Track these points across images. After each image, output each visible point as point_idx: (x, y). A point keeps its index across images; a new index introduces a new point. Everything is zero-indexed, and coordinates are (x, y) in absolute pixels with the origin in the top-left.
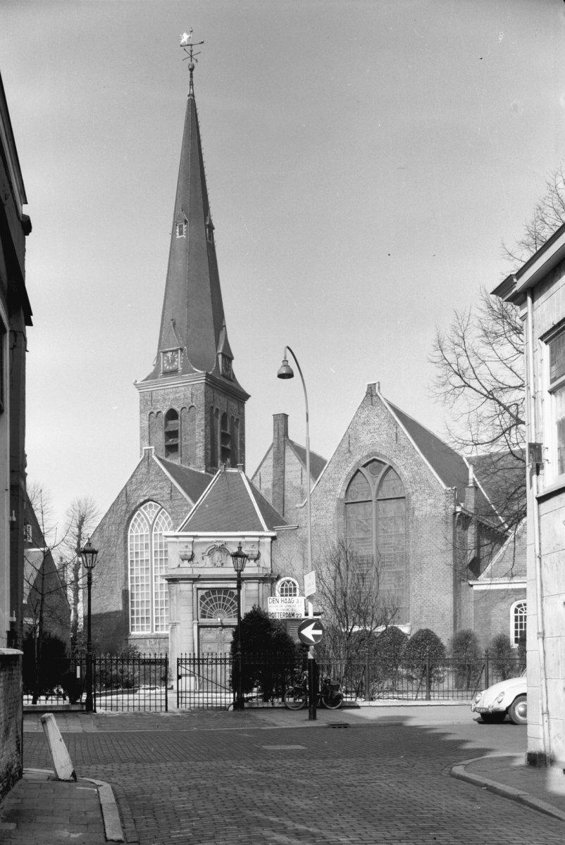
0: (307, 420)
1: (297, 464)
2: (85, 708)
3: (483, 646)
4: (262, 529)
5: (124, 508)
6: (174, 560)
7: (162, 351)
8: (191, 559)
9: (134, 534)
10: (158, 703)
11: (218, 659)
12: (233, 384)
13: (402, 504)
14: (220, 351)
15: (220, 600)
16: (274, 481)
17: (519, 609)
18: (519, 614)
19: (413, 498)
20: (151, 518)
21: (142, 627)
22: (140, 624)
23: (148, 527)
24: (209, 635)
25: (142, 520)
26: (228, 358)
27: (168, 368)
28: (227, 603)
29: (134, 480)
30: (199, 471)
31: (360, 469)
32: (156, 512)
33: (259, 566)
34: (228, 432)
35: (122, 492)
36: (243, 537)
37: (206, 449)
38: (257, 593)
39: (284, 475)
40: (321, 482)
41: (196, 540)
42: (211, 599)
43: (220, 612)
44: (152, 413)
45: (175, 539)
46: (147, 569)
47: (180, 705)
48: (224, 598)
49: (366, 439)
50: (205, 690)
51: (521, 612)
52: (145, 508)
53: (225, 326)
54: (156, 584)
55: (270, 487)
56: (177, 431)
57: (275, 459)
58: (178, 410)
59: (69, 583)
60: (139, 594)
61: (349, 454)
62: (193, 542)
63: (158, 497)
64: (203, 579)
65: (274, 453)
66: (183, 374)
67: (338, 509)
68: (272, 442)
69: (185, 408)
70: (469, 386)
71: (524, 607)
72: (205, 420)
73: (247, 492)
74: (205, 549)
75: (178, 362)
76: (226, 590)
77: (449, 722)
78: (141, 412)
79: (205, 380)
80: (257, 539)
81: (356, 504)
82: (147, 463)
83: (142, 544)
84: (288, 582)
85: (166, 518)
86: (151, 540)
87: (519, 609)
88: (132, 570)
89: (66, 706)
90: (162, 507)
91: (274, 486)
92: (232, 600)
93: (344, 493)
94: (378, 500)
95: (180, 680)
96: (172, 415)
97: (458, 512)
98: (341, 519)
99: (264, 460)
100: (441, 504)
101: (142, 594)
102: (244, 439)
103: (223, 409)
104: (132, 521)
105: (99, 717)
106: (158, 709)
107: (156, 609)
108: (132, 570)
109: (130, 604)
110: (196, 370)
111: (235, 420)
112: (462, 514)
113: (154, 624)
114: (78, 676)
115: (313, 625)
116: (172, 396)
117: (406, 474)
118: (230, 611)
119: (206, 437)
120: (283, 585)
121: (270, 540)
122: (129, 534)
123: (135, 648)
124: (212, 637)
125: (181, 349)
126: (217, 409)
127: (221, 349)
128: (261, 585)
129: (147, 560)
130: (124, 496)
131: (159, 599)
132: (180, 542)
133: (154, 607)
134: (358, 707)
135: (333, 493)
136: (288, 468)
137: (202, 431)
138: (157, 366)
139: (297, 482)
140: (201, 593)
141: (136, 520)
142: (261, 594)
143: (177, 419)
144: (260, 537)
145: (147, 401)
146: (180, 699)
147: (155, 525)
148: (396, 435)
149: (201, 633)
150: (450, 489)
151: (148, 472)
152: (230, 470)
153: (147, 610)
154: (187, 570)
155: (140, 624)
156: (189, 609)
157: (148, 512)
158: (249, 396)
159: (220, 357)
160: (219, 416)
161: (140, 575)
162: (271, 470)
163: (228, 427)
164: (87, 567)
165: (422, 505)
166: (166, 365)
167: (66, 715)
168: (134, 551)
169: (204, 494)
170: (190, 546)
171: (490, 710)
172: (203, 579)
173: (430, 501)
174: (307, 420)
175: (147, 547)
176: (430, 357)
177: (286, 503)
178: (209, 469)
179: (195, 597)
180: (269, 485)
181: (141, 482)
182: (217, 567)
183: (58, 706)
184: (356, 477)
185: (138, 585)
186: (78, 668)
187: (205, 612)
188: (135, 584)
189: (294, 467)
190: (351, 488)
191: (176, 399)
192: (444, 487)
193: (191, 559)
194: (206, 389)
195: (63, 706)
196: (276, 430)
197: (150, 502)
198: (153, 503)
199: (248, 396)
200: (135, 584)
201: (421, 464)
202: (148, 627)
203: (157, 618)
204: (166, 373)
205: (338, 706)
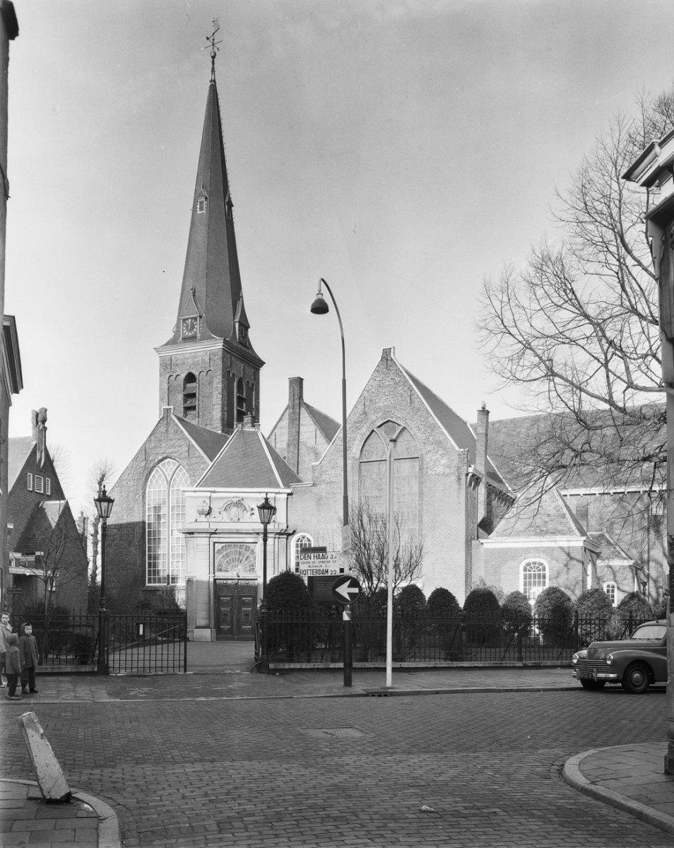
5: (143, 464)
41: (213, 495)
52: (163, 465)
82: (165, 422)
120: (298, 541)
122: (147, 490)
147: (172, 482)
151: (167, 431)
166: (185, 331)
204: (186, 339)
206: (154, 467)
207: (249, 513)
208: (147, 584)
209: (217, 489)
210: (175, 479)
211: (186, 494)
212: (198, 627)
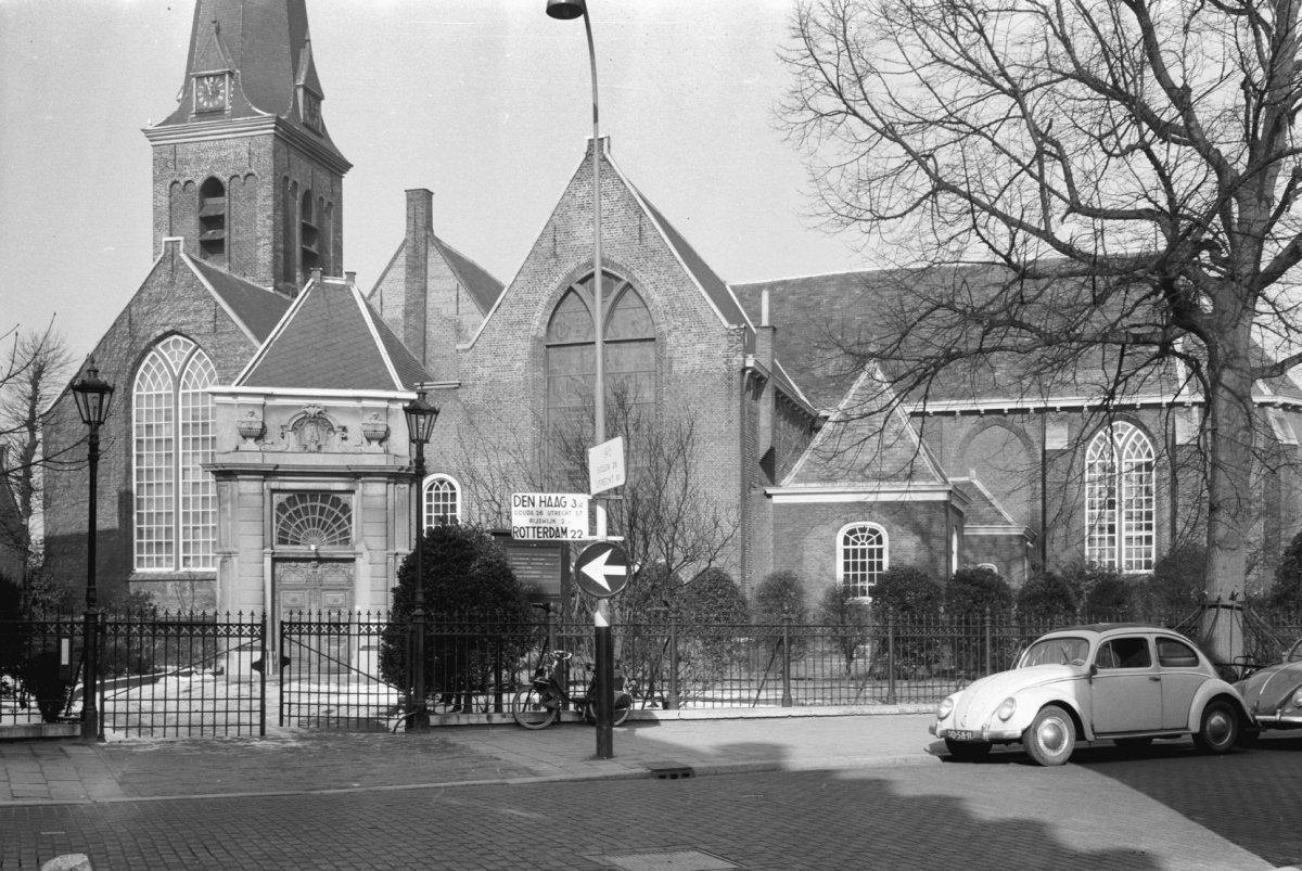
0: (596, 120)
2: (78, 732)
3: (815, 600)
4: (392, 387)
5: (126, 344)
6: (227, 438)
7: (194, 74)
8: (260, 436)
10: (245, 718)
11: (324, 624)
12: (323, 142)
13: (649, 349)
14: (301, 83)
15: (314, 512)
16: (406, 306)
17: (851, 538)
18: (851, 547)
19: (671, 340)
20: (176, 365)
22: (154, 555)
23: (170, 380)
24: (293, 576)
25: (160, 368)
26: (314, 95)
28: (327, 517)
29: (145, 295)
30: (263, 288)
31: (575, 287)
32: (187, 353)
33: (387, 452)
34: (313, 223)
35: (124, 312)
36: (359, 399)
37: (275, 250)
38: (382, 500)
39: (425, 296)
40: (502, 307)
41: (270, 402)
42: (306, 507)
43: (316, 534)
44: (175, 182)
45: (229, 399)
46: (169, 456)
47: (286, 719)
48: (322, 509)
49: (584, 233)
50: (296, 676)
51: (854, 543)
53: (309, 41)
54: (184, 483)
55: (400, 316)
56: (222, 216)
57: (408, 266)
58: (225, 179)
60: (151, 504)
61: (553, 260)
62: (264, 405)
63: (191, 327)
66: (232, 117)
67: (533, 354)
68: (403, 237)
70: (855, 114)
71: (859, 534)
72: (275, 199)
73: (363, 321)
75: (224, 95)
76: (326, 494)
77: (889, 759)
78: (155, 181)
79: (275, 129)
80: (384, 404)
81: (566, 349)
82: (169, 266)
83: (159, 412)
84: (442, 482)
85: (206, 365)
86: (177, 404)
87: (851, 538)
88: (139, 457)
89: (37, 727)
90: (199, 346)
91: (407, 314)
92: (291, 511)
93: (544, 328)
94: (606, 342)
95: (286, 668)
96: (213, 187)
97: (748, 368)
98: (539, 375)
99: (388, 269)
100: (720, 353)
102: (341, 238)
103: (304, 185)
104: (141, 370)
105: (118, 753)
106: (245, 730)
107: (184, 528)
108: (139, 457)
109: (135, 517)
110: (257, 110)
111: (325, 205)
112: (754, 372)
114: (65, 661)
115: (606, 555)
116: (213, 156)
117: (657, 299)
118: (333, 531)
119: (275, 228)
122: (135, 392)
123: (147, 597)
125: (231, 74)
126: (295, 183)
127: (303, 78)
128: (391, 485)
129: (169, 441)
131: (191, 510)
132: (239, 405)
133: (181, 525)
134: (656, 722)
135: (525, 327)
137: (268, 217)
138: (185, 102)
139: (449, 310)
140: (278, 498)
141: (147, 368)
142: (390, 503)
144: (390, 400)
145: (166, 162)
146: (286, 706)
147: (183, 379)
148: (640, 229)
149: (277, 571)
150: (736, 327)
151: (172, 283)
152: (329, 281)
153: (167, 529)
154: (252, 455)
155: (154, 555)
156: (256, 528)
157: (172, 354)
158: (351, 166)
159: (300, 92)
160: (298, 194)
161: (154, 467)
162: (402, 287)
163: (314, 214)
164: (88, 422)
165: (686, 353)
166: (201, 100)
167: (38, 748)
168: (145, 423)
169: (282, 321)
170: (259, 413)
171: (986, 735)
173: (701, 347)
174: (596, 120)
175: (168, 418)
176: (784, 53)
177: (429, 346)
178: (280, 285)
179: (267, 507)
180: (399, 314)
181: (158, 301)
182: (310, 452)
183: (16, 727)
184: (566, 300)
185: (150, 485)
186: (65, 643)
187: (286, 534)
189: (443, 287)
190: (556, 320)
191: (222, 161)
192: (726, 324)
193: (260, 436)
194: (275, 145)
195: (27, 728)
196: (411, 218)
197: (176, 337)
198: (180, 338)
199: (348, 166)
200: (145, 482)
201: (685, 281)
202: (169, 559)
204: (202, 114)
205: (622, 720)
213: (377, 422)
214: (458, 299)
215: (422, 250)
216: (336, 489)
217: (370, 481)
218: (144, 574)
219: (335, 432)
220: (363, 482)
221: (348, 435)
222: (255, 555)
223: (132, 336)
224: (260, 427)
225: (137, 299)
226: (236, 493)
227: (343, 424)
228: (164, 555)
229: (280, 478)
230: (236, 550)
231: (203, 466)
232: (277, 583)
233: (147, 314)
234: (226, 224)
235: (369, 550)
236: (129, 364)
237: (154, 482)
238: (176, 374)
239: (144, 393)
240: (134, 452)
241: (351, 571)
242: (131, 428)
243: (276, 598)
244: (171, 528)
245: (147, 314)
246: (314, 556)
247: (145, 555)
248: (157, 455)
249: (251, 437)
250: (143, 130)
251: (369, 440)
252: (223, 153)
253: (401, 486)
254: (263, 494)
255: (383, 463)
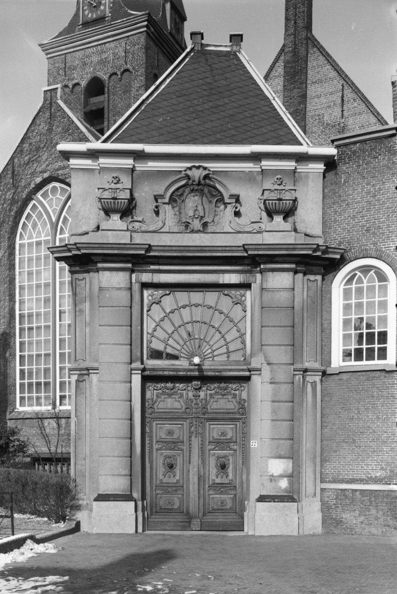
1: (332, 79)
5: (9, 195)
8: (127, 210)
9: (26, 241)
21: (38, 398)
22: (35, 395)
25: (40, 216)
27: (90, 16)
29: (26, 145)
41: (141, 167)
52: (45, 195)
57: (286, 73)
58: (105, 77)
59: (53, 411)
62: (133, 170)
64: (158, 260)
65: (286, 63)
68: (282, 42)
69: (115, 74)
74: (163, 189)
79: (147, 26)
82: (48, 114)
96: (96, 87)
101: (38, 342)
107: (61, 369)
110: (132, 12)
113: (58, 394)
116: (95, 59)
120: (350, 281)
121: (320, 167)
122: (18, 242)
123: (13, 433)
124: (177, 405)
128: (300, 275)
130: (10, 176)
136: (312, 91)
141: (29, 217)
143: (103, 93)
147: (60, 224)
149: (148, 395)
151: (50, 130)
155: (35, 395)
166: (86, 12)
170: (126, 182)
172: (158, 260)
181: (38, 149)
182: (193, 231)
185: (30, 329)
188: (26, 326)
198: (57, 185)
203: (62, 384)
204: (86, 24)
206: (29, 199)
207: (230, 210)
208: (21, 409)
209: (150, 148)
210: (65, 219)
211: (73, 162)
212: (101, 498)
213: (281, 187)
214: (343, 100)
215: (302, 51)
216: (226, 282)
217: (273, 270)
218: (25, 413)
219: (226, 204)
220: (261, 272)
221: (242, 210)
222: (121, 371)
223: (15, 186)
224: (128, 196)
225: (19, 151)
226: (96, 289)
227: (234, 191)
228: (43, 394)
229: (152, 267)
230: (95, 365)
231: (53, 250)
232: (148, 411)
233: (28, 163)
234: (106, 116)
235: (269, 364)
236: (13, 213)
237: (34, 325)
238: (54, 219)
239: (26, 241)
240: (17, 298)
241: (244, 395)
242: (14, 275)
243: (147, 429)
244: (49, 369)
245: (28, 163)
246: (196, 373)
247: (26, 395)
248: (37, 299)
249: (115, 211)
250: (40, 45)
251: (270, 214)
252: (104, 56)
253: (312, 277)
254: (131, 289)
255: (291, 241)
